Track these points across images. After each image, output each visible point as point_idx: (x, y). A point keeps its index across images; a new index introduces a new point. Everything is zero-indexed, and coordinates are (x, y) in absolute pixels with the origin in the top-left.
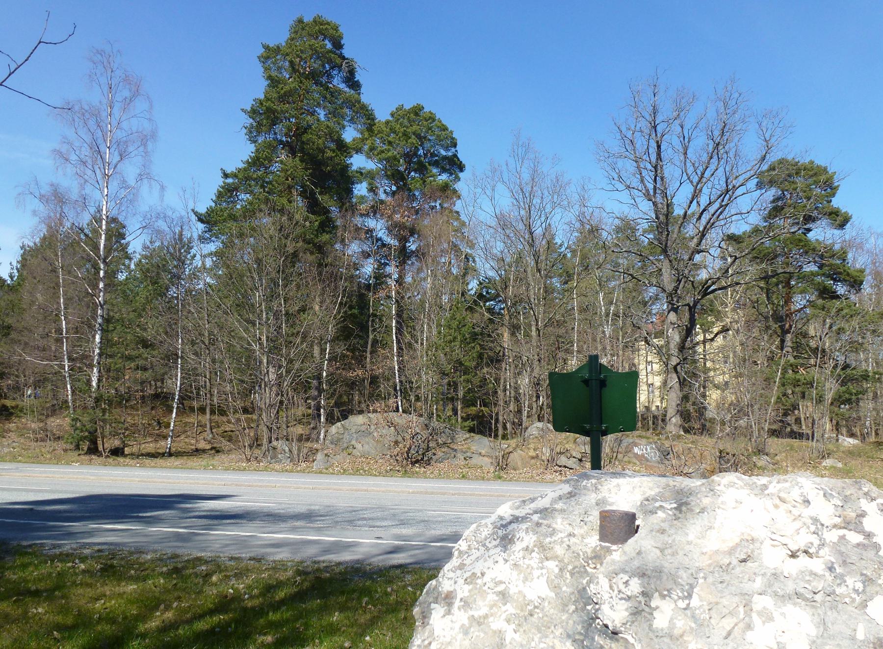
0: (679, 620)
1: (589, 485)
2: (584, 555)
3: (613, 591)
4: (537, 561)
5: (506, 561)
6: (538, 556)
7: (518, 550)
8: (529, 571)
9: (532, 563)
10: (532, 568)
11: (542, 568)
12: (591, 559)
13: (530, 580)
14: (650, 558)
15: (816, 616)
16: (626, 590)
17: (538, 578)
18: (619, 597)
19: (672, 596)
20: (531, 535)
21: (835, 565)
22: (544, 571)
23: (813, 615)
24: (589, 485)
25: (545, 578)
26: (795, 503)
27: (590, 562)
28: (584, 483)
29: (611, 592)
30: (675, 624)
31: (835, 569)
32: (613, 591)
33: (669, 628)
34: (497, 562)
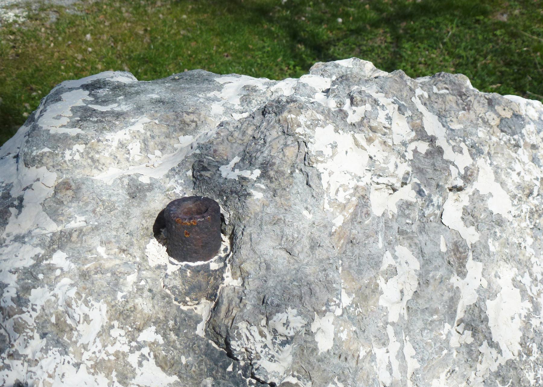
0: (342, 331)
1: (77, 157)
2: (174, 293)
3: (265, 337)
4: (125, 340)
5: (77, 365)
6: (123, 332)
7: (92, 340)
8: (121, 361)
9: (118, 347)
10: (123, 354)
11: (139, 348)
12: (187, 294)
13: (129, 375)
14: (280, 267)
15: (414, 247)
16: (288, 330)
17: (140, 364)
18: (278, 341)
19: (331, 308)
20: (96, 304)
21: (422, 187)
22: (145, 351)
23: (410, 246)
24: (77, 157)
25: (152, 361)
26: (385, 130)
27: (188, 299)
28: (68, 157)
29: (263, 339)
30: (340, 338)
31: (424, 192)
32: (265, 337)
33: (335, 345)
34: (63, 375)
